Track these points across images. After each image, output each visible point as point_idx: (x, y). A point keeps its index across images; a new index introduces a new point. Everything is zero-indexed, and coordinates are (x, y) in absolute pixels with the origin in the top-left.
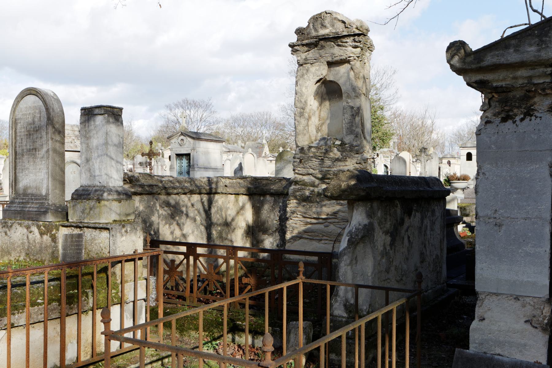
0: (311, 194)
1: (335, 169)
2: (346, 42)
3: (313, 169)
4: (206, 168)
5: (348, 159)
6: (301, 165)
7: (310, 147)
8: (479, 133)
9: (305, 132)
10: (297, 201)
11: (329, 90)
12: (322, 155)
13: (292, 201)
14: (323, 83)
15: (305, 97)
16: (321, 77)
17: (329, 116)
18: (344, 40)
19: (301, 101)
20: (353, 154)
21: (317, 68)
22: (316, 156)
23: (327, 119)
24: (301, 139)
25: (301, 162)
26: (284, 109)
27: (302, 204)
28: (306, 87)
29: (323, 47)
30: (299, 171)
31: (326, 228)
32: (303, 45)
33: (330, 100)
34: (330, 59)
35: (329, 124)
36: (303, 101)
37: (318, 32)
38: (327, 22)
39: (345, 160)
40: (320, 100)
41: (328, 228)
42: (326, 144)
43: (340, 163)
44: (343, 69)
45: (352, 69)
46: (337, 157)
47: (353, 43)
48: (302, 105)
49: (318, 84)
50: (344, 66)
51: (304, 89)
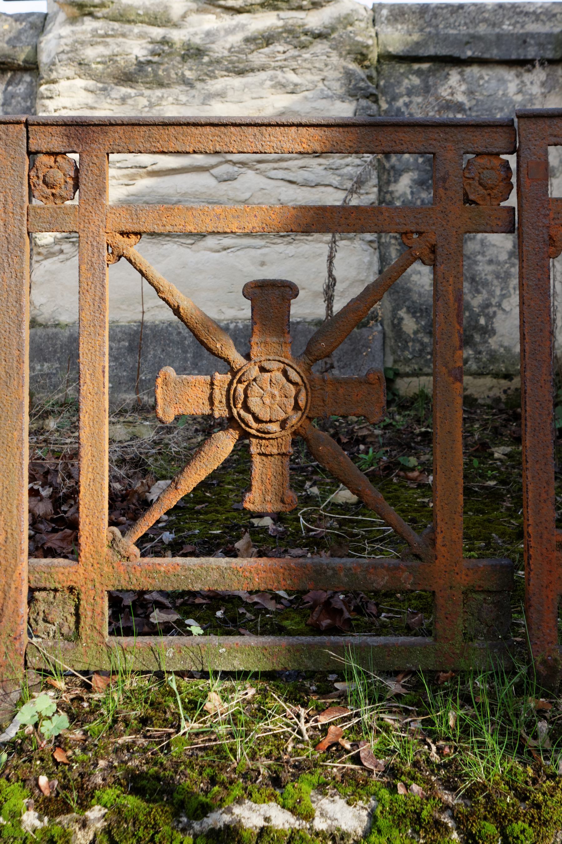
0: (153, 53)
10: (91, 83)
13: (63, 84)
27: (114, 94)
31: (224, 186)
41: (234, 184)
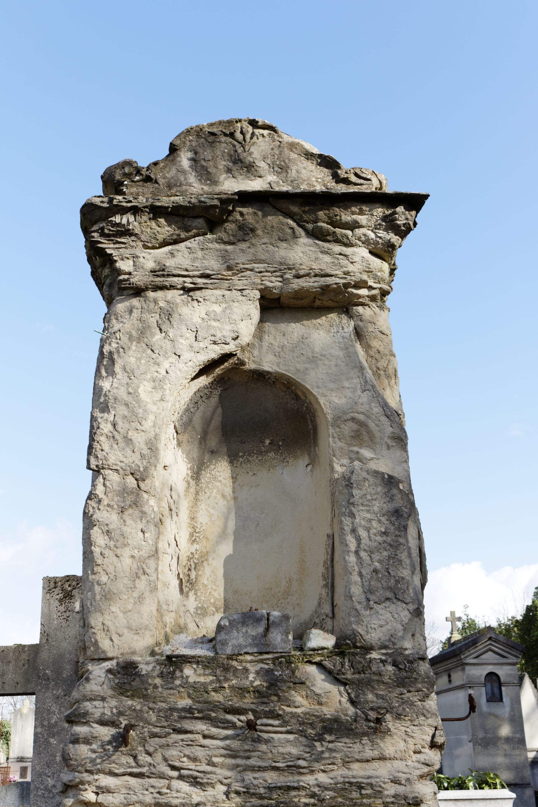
1: (323, 778)
2: (354, 226)
3: (195, 782)
4: (307, 297)
5: (389, 721)
6: (123, 760)
7: (174, 662)
8: (426, 648)
9: (142, 584)
11: (253, 415)
12: (248, 701)
14: (220, 381)
15: (148, 425)
16: (227, 349)
17: (232, 525)
18: (346, 217)
19: (128, 441)
20: (414, 697)
21: (217, 309)
22: (215, 706)
23: (222, 536)
24: (122, 619)
25: (121, 740)
26: (269, 333)
28: (158, 384)
29: (246, 232)
30: (100, 790)
32: (157, 212)
33: (233, 458)
34: (273, 283)
35: (228, 561)
36: (139, 439)
37: (215, 183)
38: (259, 148)
39: (376, 728)
40: (195, 454)
42: (263, 647)
43: (343, 745)
44: (323, 333)
45: (359, 333)
46: (328, 711)
47: (382, 233)
48: (133, 459)
49: (204, 381)
50: (323, 320)
51: (144, 390)
